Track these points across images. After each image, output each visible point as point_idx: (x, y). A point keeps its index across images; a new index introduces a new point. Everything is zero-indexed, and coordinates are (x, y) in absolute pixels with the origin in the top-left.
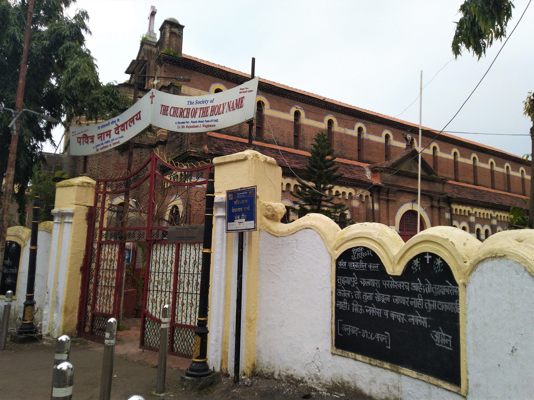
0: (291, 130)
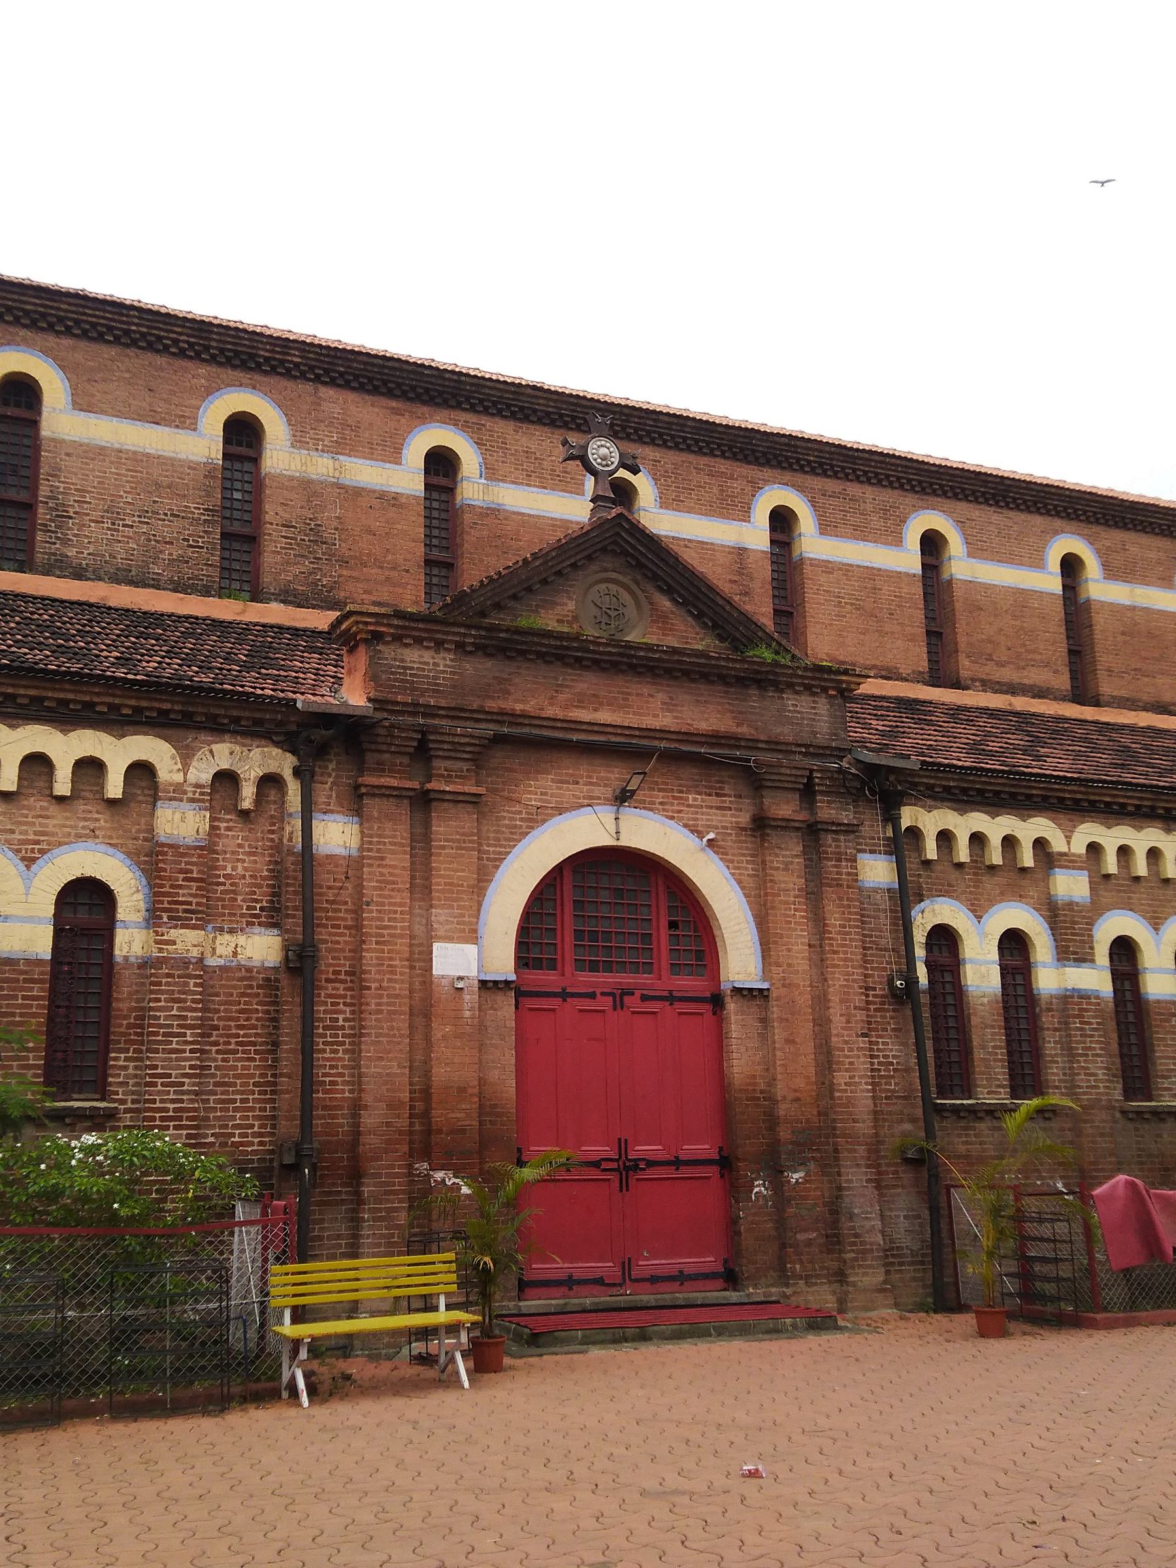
0: (1052, 640)
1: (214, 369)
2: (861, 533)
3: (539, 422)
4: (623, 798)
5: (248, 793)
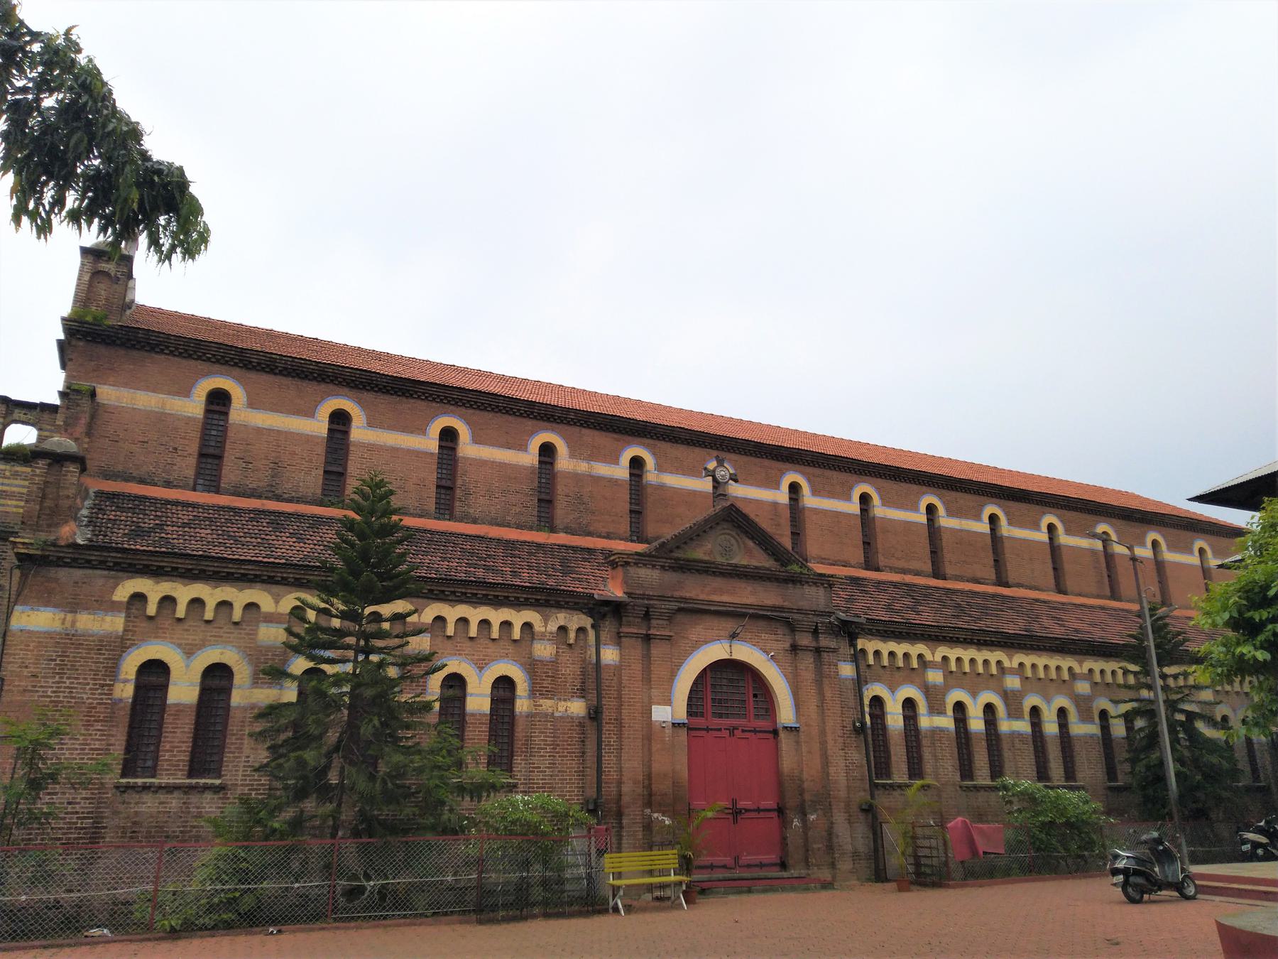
1: (535, 422)
2: (832, 495)
3: (682, 443)
4: (733, 636)
5: (572, 635)
